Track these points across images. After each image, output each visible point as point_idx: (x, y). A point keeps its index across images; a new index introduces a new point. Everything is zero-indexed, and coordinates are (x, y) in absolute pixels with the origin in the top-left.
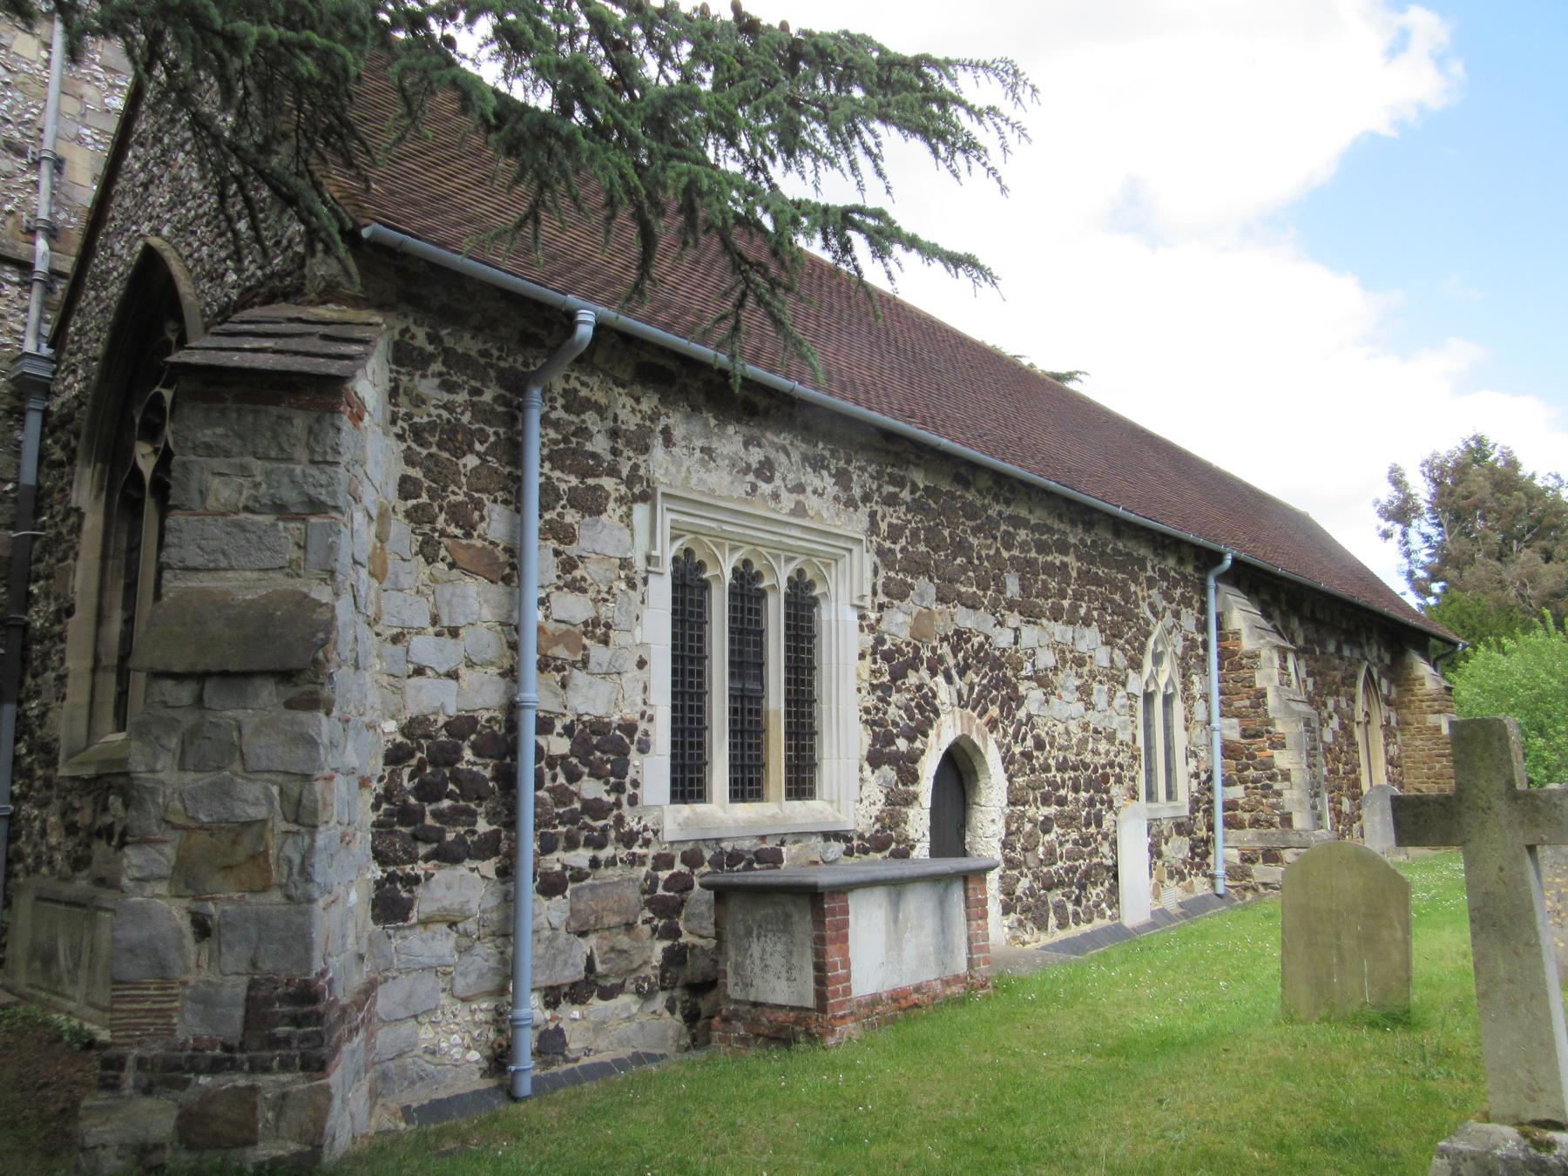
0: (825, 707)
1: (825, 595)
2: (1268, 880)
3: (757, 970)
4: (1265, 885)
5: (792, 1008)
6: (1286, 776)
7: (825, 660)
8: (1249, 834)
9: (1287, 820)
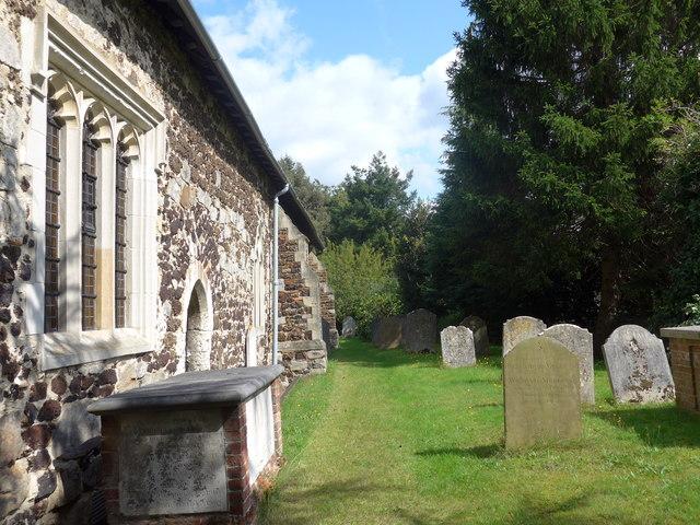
0: (134, 252)
1: (136, 158)
2: (298, 369)
3: (157, 485)
4: (296, 371)
5: (209, 513)
6: (309, 310)
7: (135, 211)
8: (288, 344)
9: (309, 335)
